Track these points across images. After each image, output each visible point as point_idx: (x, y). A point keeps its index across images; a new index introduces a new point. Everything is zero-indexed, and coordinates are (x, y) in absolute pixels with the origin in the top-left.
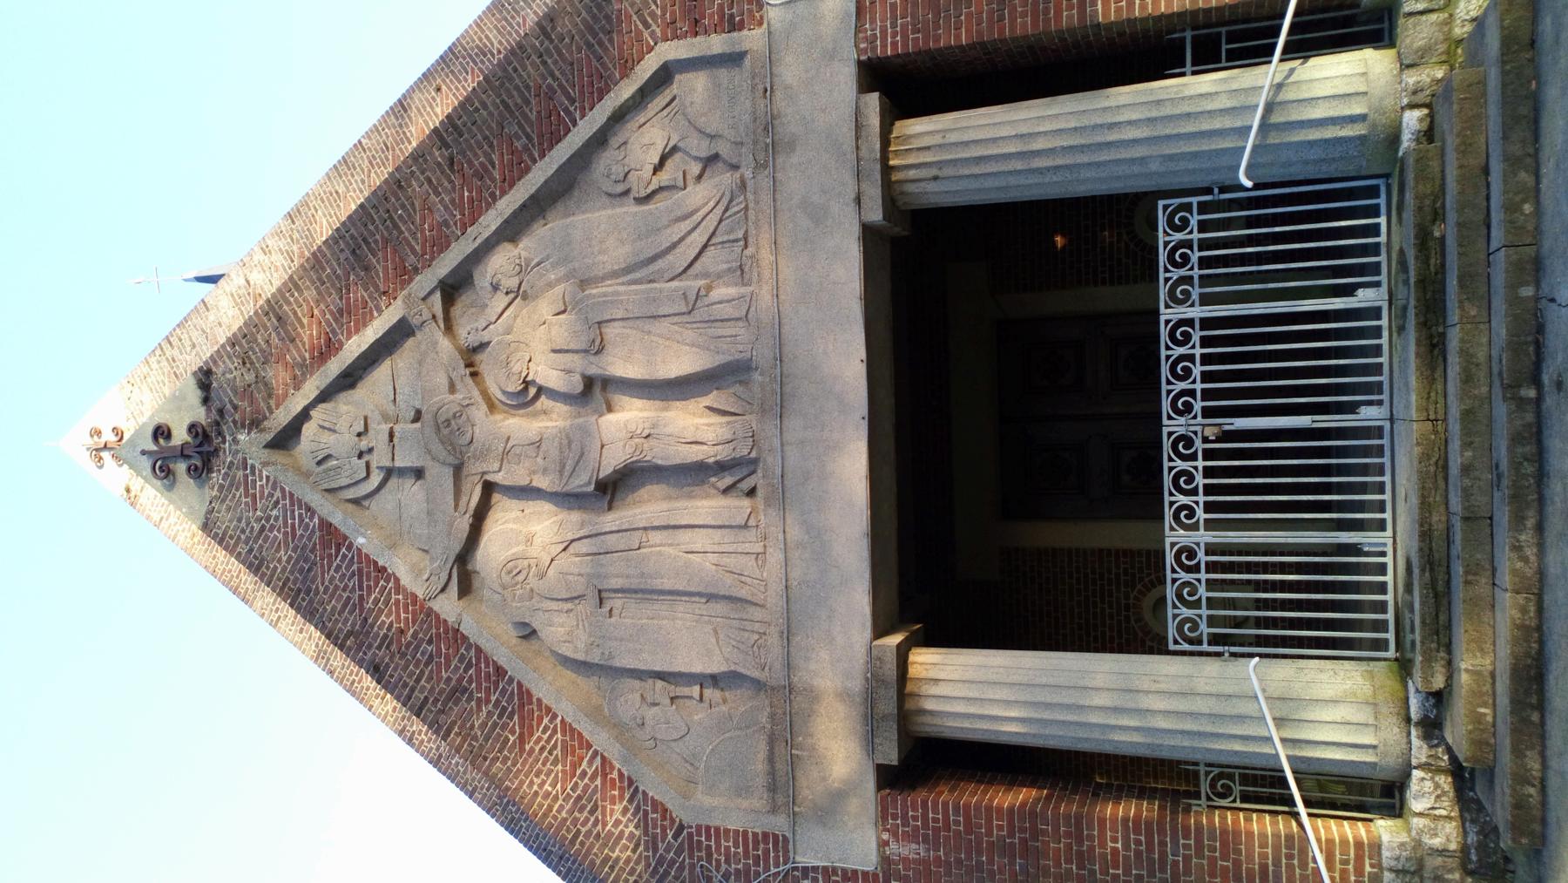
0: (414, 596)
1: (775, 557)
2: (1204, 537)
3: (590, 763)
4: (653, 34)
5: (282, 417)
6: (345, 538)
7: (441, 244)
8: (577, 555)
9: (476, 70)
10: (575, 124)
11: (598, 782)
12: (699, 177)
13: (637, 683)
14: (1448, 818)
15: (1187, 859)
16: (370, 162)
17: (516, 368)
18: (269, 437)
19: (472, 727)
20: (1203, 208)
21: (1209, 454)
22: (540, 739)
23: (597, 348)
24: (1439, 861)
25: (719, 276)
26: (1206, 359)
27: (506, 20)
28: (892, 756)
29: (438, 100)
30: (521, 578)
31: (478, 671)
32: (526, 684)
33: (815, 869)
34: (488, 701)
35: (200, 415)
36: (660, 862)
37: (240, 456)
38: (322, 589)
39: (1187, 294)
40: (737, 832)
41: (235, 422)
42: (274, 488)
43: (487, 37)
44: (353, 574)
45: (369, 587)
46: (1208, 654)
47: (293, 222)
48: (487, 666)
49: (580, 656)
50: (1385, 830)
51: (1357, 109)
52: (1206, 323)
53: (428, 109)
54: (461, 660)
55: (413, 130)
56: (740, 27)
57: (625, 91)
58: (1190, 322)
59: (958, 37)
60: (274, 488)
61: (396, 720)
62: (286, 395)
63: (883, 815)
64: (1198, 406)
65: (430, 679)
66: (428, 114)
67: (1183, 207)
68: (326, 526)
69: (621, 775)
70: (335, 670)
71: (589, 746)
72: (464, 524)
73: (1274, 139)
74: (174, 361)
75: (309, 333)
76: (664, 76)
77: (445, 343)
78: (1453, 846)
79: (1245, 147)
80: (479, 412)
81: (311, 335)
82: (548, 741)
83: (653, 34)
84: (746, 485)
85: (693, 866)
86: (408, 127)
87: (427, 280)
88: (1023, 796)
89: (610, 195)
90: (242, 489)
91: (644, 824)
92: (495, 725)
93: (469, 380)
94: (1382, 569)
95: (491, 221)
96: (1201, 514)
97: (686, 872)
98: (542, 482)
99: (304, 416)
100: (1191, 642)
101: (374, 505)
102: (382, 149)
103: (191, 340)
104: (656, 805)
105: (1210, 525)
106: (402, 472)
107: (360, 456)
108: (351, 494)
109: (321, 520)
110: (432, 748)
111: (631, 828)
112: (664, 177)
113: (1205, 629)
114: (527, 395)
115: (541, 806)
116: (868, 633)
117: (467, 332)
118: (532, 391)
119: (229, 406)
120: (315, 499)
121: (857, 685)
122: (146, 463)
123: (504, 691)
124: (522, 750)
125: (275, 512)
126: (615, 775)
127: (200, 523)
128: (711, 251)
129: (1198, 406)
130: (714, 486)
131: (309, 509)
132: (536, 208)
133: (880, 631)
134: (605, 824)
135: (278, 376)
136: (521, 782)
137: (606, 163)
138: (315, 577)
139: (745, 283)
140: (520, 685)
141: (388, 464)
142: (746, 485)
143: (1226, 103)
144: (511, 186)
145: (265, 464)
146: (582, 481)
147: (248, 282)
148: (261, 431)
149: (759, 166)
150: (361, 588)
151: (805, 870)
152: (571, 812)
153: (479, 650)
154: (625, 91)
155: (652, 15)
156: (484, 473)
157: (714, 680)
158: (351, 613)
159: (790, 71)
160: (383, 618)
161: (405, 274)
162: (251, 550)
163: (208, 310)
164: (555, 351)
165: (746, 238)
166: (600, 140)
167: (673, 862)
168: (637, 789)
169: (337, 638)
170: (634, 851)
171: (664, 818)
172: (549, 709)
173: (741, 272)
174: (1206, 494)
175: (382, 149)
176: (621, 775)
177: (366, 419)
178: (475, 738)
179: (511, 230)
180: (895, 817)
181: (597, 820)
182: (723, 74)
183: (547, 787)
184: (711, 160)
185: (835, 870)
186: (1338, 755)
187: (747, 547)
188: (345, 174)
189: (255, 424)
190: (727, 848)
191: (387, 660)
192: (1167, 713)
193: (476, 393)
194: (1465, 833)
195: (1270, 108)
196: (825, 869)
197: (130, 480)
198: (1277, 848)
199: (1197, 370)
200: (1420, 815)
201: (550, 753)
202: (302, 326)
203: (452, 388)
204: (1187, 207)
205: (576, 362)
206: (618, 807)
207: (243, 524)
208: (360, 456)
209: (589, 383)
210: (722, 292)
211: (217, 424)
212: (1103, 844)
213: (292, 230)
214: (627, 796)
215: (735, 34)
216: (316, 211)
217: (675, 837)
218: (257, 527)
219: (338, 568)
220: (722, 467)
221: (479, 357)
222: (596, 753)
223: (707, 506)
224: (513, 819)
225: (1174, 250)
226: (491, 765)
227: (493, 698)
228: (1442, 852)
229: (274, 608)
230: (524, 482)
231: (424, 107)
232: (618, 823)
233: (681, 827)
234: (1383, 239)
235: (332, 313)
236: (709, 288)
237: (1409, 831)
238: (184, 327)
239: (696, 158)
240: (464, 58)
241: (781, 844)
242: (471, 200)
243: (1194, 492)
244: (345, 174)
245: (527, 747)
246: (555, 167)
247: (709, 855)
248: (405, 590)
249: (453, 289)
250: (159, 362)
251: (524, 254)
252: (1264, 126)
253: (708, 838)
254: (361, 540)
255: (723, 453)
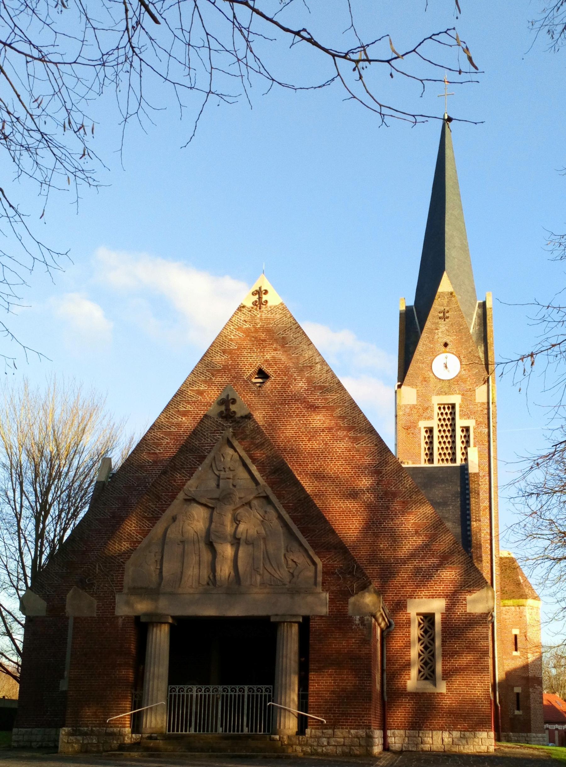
0: (184, 485)
1: (191, 591)
2: (195, 694)
3: (140, 538)
4: (325, 561)
5: (236, 443)
6: (201, 463)
7: (279, 497)
8: (194, 535)
9: (381, 460)
10: (306, 538)
11: (135, 540)
12: (289, 572)
13: (160, 551)
14: (131, 741)
15: (121, 688)
16: (354, 417)
17: (244, 519)
18: (230, 439)
19: (149, 502)
20: (270, 696)
21: (213, 696)
22: (146, 523)
23: (247, 543)
24: (122, 739)
25: (263, 578)
26: (235, 695)
27: (396, 473)
28: (143, 620)
29: (373, 445)
30: (188, 518)
31: (164, 505)
32: (161, 519)
33: (115, 599)
34: (156, 507)
35: (238, 415)
36: (115, 557)
37: (226, 429)
38: (187, 455)
39: (250, 692)
40: (123, 578)
41: (235, 427)
42: (216, 440)
43: (391, 465)
44: (191, 466)
45: (187, 470)
46: (168, 694)
47: (336, 384)
48: (166, 507)
49: (167, 535)
50: (128, 730)
51: (282, 727)
52: (243, 696)
53: (370, 441)
54: (167, 499)
55: (364, 435)
56: (323, 585)
57: (311, 553)
58: (244, 692)
59: (311, 640)
60: (216, 440)
61: (158, 423)
62: (242, 445)
63: (128, 617)
64: (225, 693)
65: (162, 489)
66: (368, 441)
67: (270, 691)
68: (204, 457)
69: (137, 546)
70: (176, 398)
71: (144, 537)
72: (203, 501)
73: (279, 710)
74: (290, 329)
75: (258, 454)
76: (314, 564)
77: (251, 497)
78: (125, 742)
79: (277, 704)
80: (232, 507)
81: (258, 454)
82: (146, 525)
83: (325, 561)
84: (210, 583)
85: (114, 566)
86: (365, 432)
87: (269, 491)
88: (133, 651)
89: (287, 548)
90: (216, 429)
91: (124, 553)
92: (150, 509)
93: (242, 504)
94: (186, 731)
95: (284, 513)
96: (199, 694)
97: (113, 564)
98: (213, 525)
99: (236, 451)
100: (171, 690)
101: (210, 471)
102: (358, 422)
103: (298, 337)
104: (129, 556)
105: (197, 696)
106: (219, 480)
107: (224, 468)
108: (213, 465)
109: (206, 455)
110: (149, 437)
111: (123, 549)
112: (290, 562)
113: (173, 694)
114: (236, 521)
115: (129, 523)
116: (172, 615)
117: (255, 503)
118: (237, 522)
119: (240, 425)
120: (212, 454)
121: (159, 611)
122: (224, 396)
123: (159, 512)
124: (144, 517)
125: (209, 440)
126: (137, 545)
127: (209, 414)
128: (269, 575)
129: (225, 693)
130: (211, 574)
131: (210, 451)
132: (285, 525)
133: (173, 617)
134: (124, 541)
135: (246, 443)
136: (134, 517)
137: (295, 545)
138: (191, 453)
139: (260, 585)
140: (160, 517)
141: (221, 478)
142: (210, 583)
143: (287, 700)
144: (292, 518)
145: (223, 437)
146: (213, 537)
147: (317, 363)
148: (232, 437)
149: (288, 589)
150: (187, 468)
151: (114, 597)
152: (127, 531)
153: (169, 505)
154: (311, 553)
155: (329, 561)
156: (216, 507)
157: (161, 572)
158: (181, 465)
159: (310, 599)
160: (179, 475)
161: (272, 484)
162: (199, 431)
163: (308, 345)
164: (247, 530)
165: (271, 585)
166: (301, 545)
167: (115, 561)
168: (133, 551)
169: (174, 460)
170: (118, 550)
171: (126, 558)
172: (154, 525)
173: (263, 584)
174: (204, 695)
175: (358, 422)
176: (137, 546)
177: (234, 470)
178: (146, 503)
179: (280, 517)
180: (128, 620)
181: (125, 539)
182: (313, 580)
183: (134, 525)
184: (292, 574)
185: (115, 604)
186: (144, 720)
187: (194, 583)
188: (351, 406)
189: (234, 435)
190: (119, 576)
191: (168, 476)
192: (153, 684)
193: (238, 506)
194: (128, 744)
195: (285, 709)
196: (115, 602)
197: (248, 308)
198: (124, 707)
199: (233, 694)
200: (132, 736)
201: (142, 526)
202: (261, 451)
203: (240, 498)
204: (270, 692)
205: (244, 535)
206: (129, 546)
207: (207, 429)
208: (224, 468)
209: (239, 539)
210: (258, 578)
211: (235, 421)
212: (123, 669)
213: (334, 383)
214: (132, 548)
215: (321, 584)
216: (340, 394)
217: (121, 561)
218: (205, 434)
219: (193, 461)
220: (214, 576)
221: (248, 506)
222: (142, 539)
223: (205, 573)
224: (125, 468)
225: (261, 689)
226: (139, 508)
227: (157, 509)
228: (124, 740)
229: (198, 372)
230: (213, 520)
231: (371, 439)
232: (125, 545)
233: (124, 563)
234: (258, 733)
235: (263, 461)
236: (260, 575)
237: (129, 734)
238: (303, 334)
239: (294, 571)
240: (385, 456)
241: (120, 591)
242: (289, 506)
243: (205, 692)
244: (351, 406)
245: (144, 519)
246: (295, 532)
247: (117, 571)
248: (186, 482)
249: (267, 498)
250: (291, 322)
251: (273, 522)
252: (281, 708)
253: (121, 571)
254: (200, 469)
255: (218, 578)
